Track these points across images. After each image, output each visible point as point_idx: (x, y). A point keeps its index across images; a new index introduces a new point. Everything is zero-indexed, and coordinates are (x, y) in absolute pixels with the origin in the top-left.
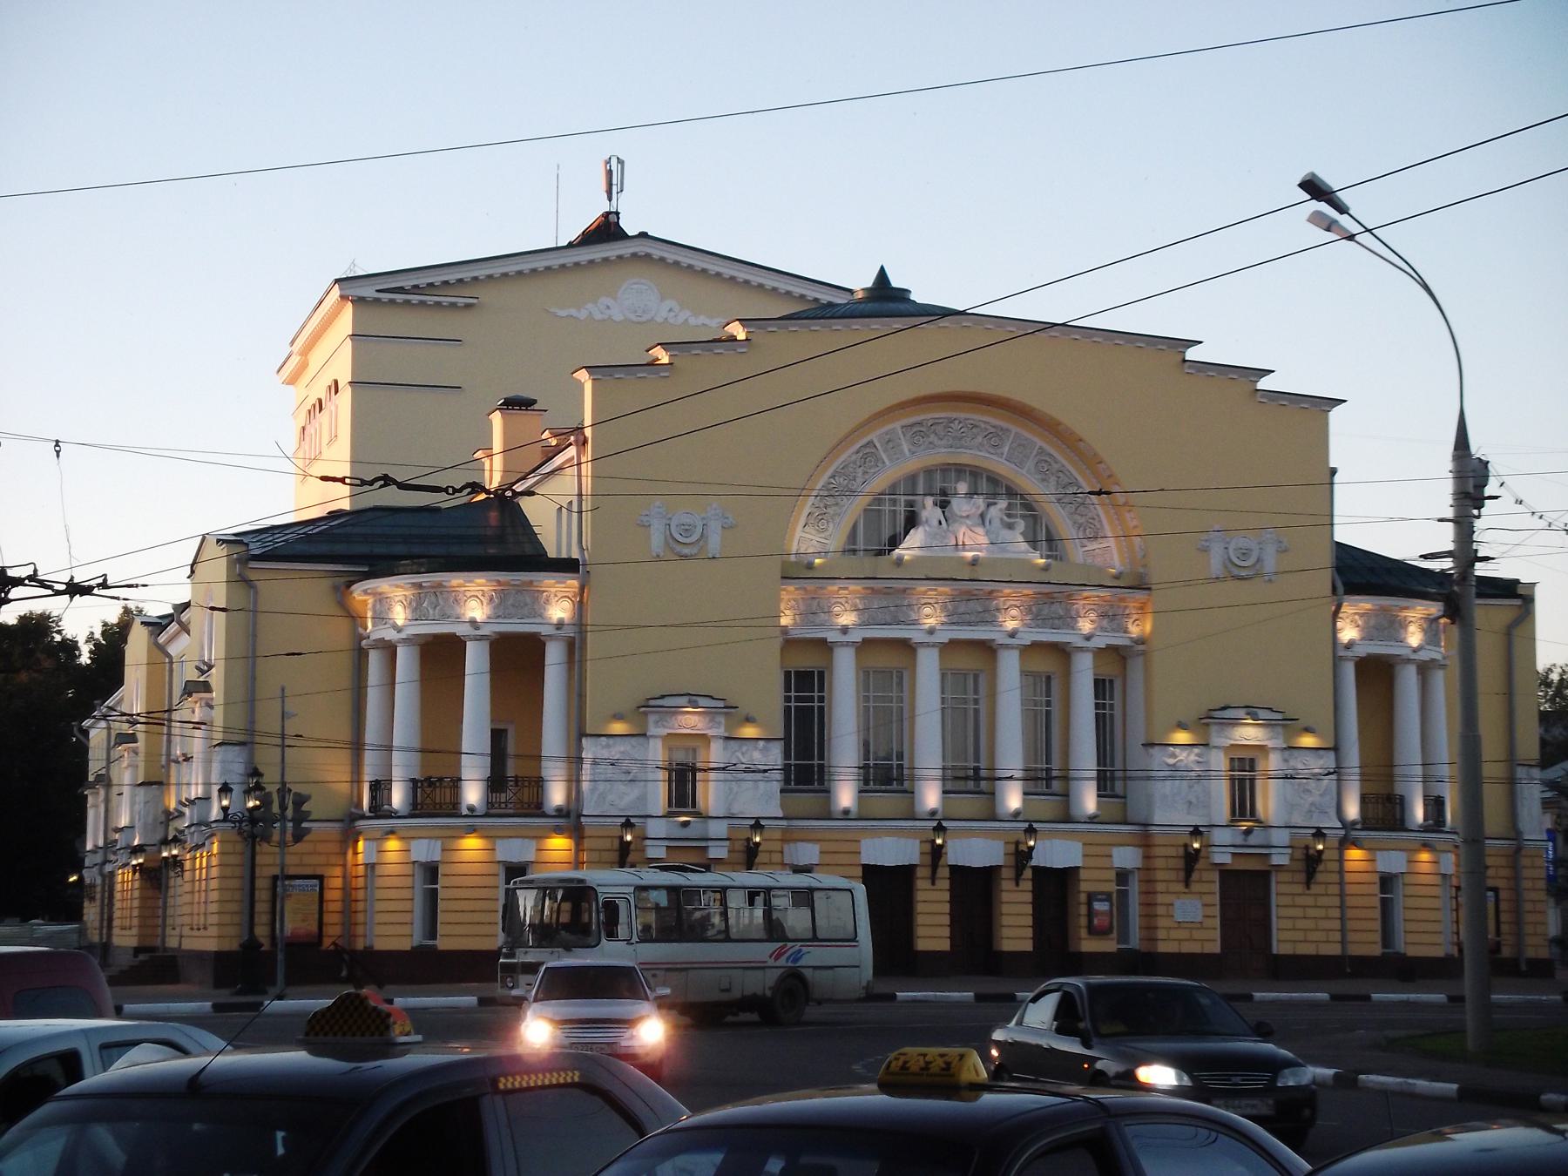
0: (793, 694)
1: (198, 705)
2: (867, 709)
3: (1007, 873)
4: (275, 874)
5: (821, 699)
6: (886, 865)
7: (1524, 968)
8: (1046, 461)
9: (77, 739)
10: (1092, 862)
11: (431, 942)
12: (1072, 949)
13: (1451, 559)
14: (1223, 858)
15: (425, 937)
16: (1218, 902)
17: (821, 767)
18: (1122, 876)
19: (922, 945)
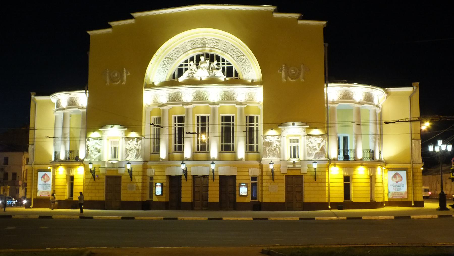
0: (231, 126)
1: (279, 145)
6: (226, 175)
13: (299, 24)
17: (233, 145)
19: (183, 200)
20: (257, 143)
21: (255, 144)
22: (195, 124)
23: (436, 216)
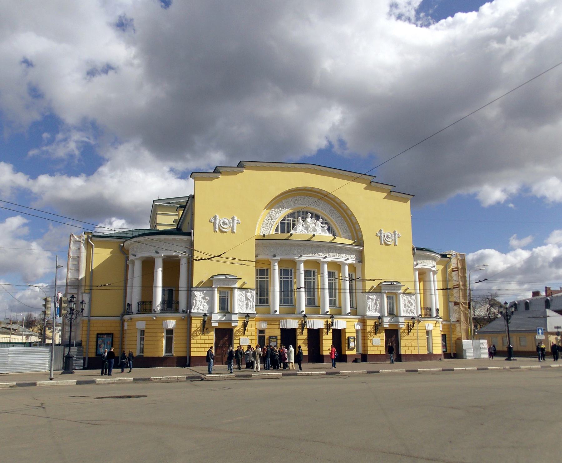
2: (281, 281)
3: (325, 330)
5: (257, 278)
7: (452, 356)
8: (332, 210)
10: (349, 327)
11: (141, 354)
12: (400, 353)
14: (386, 326)
20: (292, 296)
21: (283, 297)
22: (294, 273)
23: (540, 367)
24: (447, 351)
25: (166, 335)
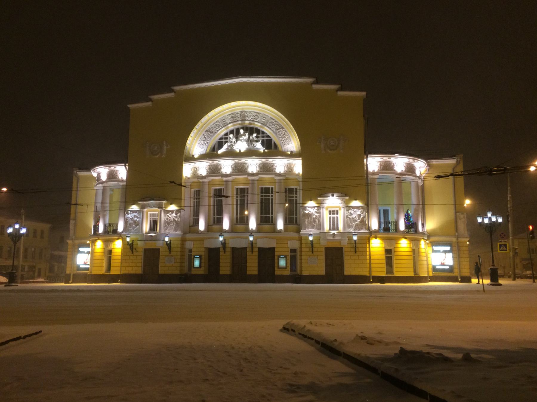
3: (222, 250)
4: (89, 251)
9: (354, 225)
15: (189, 271)
16: (160, 256)
17: (272, 217)
18: (293, 251)
19: (248, 273)
24: (194, 269)
25: (391, 256)
